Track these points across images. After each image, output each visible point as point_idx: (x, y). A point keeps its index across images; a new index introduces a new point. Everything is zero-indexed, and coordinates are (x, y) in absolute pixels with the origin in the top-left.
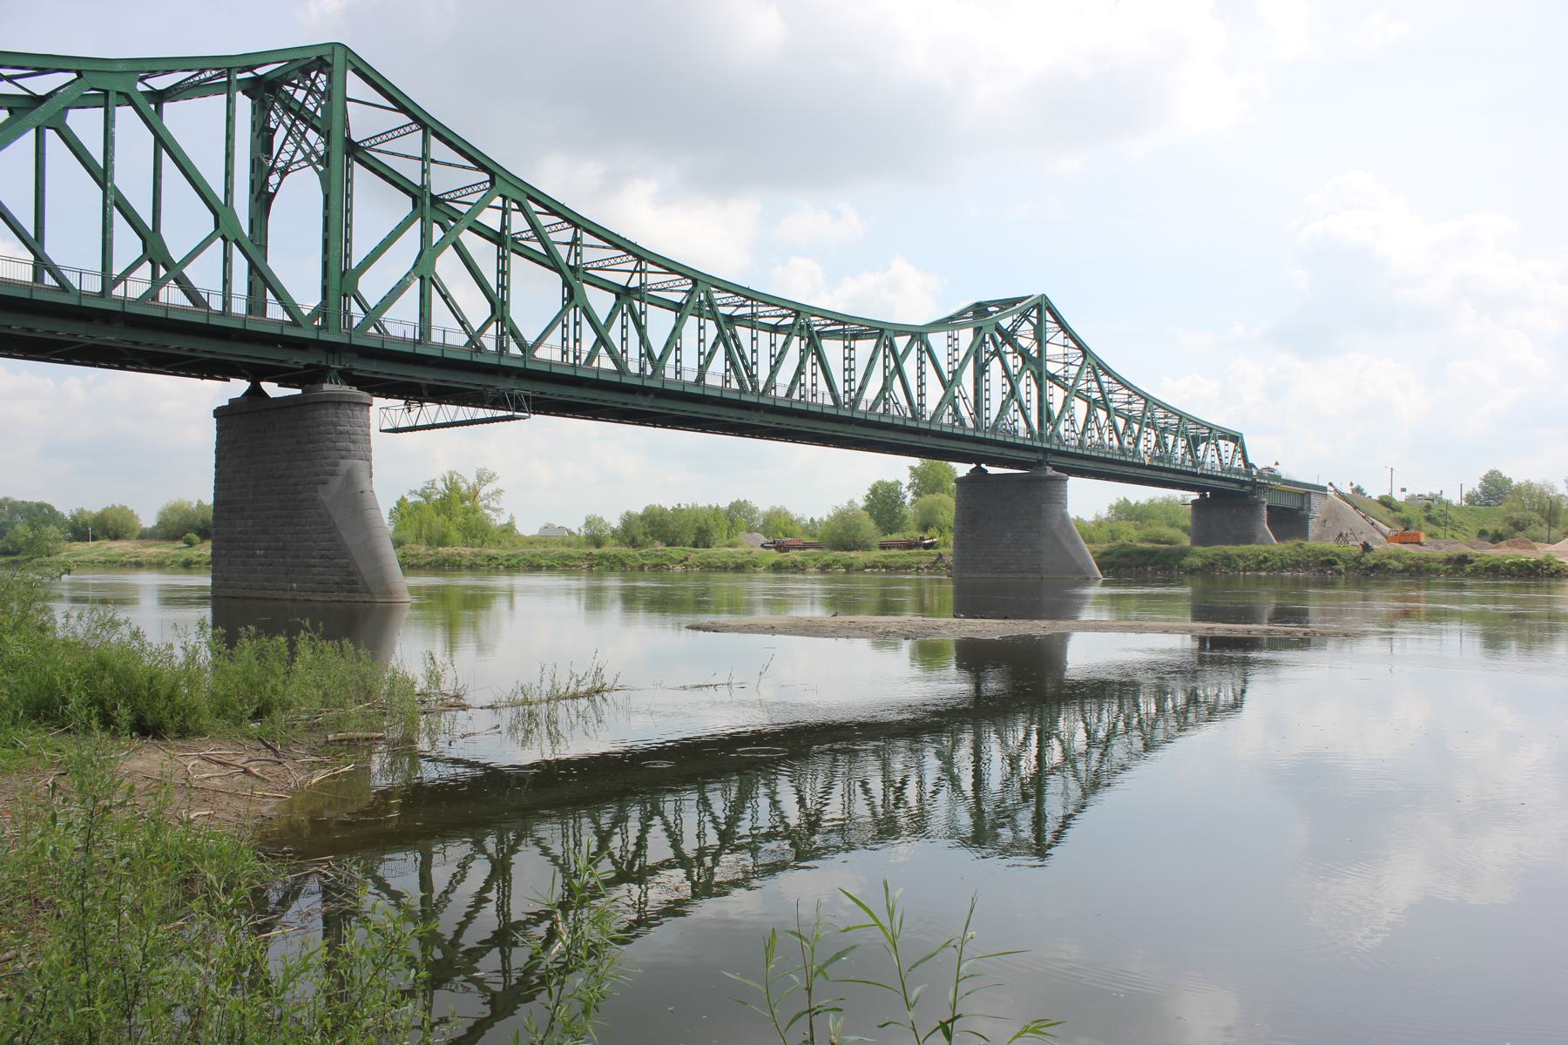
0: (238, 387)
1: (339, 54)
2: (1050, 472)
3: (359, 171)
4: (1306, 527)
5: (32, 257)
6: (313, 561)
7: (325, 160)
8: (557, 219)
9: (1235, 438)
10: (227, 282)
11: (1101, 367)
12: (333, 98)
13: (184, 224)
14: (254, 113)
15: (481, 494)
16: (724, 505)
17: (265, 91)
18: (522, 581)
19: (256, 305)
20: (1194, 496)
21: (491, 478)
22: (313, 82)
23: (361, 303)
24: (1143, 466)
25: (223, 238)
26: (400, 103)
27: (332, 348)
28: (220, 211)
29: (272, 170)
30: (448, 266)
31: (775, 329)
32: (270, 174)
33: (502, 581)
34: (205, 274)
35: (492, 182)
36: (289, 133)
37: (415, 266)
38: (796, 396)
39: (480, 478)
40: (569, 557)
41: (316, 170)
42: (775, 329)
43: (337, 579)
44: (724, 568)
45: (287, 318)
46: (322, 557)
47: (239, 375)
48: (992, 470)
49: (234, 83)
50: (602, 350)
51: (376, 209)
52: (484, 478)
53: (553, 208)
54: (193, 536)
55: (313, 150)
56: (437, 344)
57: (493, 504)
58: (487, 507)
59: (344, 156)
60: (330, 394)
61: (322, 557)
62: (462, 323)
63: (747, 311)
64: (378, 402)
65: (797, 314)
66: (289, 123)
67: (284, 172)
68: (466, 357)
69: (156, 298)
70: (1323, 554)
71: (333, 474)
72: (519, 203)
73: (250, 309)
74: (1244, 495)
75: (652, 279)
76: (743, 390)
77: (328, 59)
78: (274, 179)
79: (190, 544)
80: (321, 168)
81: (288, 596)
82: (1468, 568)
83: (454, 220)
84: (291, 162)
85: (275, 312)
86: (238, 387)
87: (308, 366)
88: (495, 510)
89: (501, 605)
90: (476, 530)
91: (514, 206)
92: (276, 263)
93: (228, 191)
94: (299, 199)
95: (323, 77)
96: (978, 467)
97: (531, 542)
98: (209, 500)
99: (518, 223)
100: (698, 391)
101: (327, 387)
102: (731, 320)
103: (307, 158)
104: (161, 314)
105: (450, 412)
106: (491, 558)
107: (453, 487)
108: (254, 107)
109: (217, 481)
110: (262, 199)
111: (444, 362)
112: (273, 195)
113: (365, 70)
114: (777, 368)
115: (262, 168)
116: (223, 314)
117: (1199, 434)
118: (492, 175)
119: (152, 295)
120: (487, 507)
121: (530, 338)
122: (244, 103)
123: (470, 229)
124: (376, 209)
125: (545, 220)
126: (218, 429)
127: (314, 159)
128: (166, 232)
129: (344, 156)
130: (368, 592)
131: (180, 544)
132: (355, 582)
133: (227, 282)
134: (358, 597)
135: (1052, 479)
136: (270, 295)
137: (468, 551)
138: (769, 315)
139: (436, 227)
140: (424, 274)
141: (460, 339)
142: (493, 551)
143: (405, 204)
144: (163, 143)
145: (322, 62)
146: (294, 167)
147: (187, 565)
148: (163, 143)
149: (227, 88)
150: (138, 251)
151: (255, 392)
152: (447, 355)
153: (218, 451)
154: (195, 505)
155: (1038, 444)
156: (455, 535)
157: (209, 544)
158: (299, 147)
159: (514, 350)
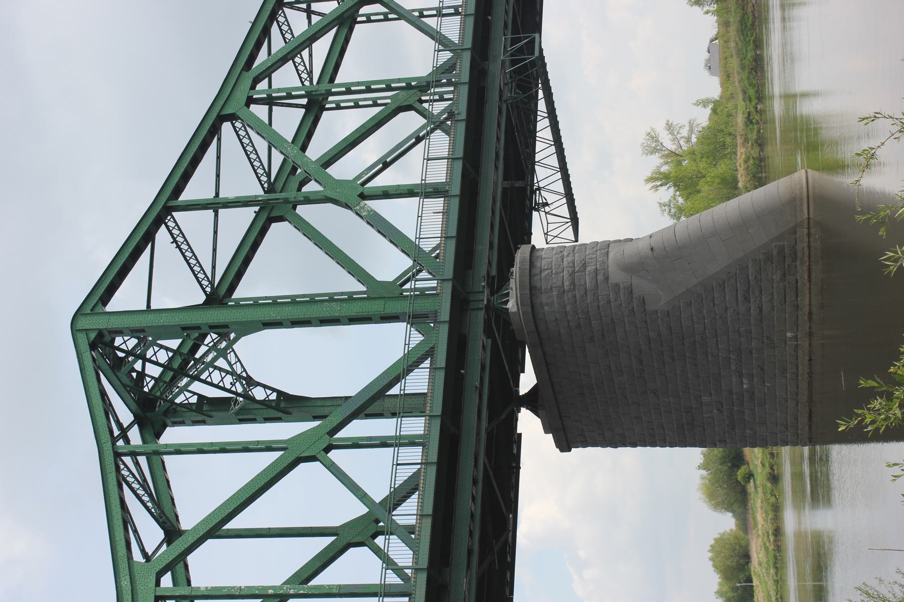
0: (528, 423)
1: (83, 323)
3: (240, 293)
6: (754, 312)
7: (223, 330)
8: (275, 29)
10: (383, 443)
12: (148, 326)
13: (313, 497)
14: (182, 423)
15: (672, 147)
17: (154, 412)
18: (776, 88)
19: (410, 406)
21: (653, 137)
22: (129, 353)
23: (409, 276)
25: (328, 449)
26: (141, 241)
27: (461, 303)
28: (293, 458)
29: (246, 396)
30: (347, 169)
32: (253, 399)
33: (777, 108)
34: (377, 472)
35: (232, 118)
36: (196, 378)
37: (347, 206)
39: (654, 151)
40: (742, 22)
41: (236, 340)
43: (777, 277)
45: (427, 363)
46: (747, 299)
47: (512, 421)
49: (151, 447)
51: (284, 267)
52: (653, 146)
53: (260, 34)
54: (741, 473)
55: (214, 347)
56: (450, 172)
57: (685, 132)
58: (688, 140)
59: (223, 311)
60: (521, 303)
61: (747, 299)
62: (419, 140)
64: (537, 239)
66: (186, 380)
67: (250, 382)
68: (461, 128)
69: (411, 529)
71: (630, 291)
72: (257, 80)
73: (420, 412)
77: (93, 336)
78: (259, 394)
79: (750, 476)
80: (232, 336)
81: (804, 343)
83: (294, 169)
84: (233, 373)
85: (418, 381)
86: (528, 423)
87: (488, 332)
88: (691, 131)
89: (808, 108)
90: (715, 144)
91: (263, 85)
92: (350, 383)
93: (268, 447)
94: (275, 359)
95: (118, 341)
97: (726, 78)
98: (694, 455)
99: (286, 78)
101: (511, 305)
103: (223, 354)
104: (428, 522)
105: (544, 151)
106: (749, 121)
107: (660, 179)
108: (175, 424)
109: (653, 445)
110: (286, 406)
111: (470, 160)
112: (280, 393)
113: (102, 290)
115: (242, 406)
118: (222, 118)
119: (406, 533)
120: (688, 140)
122: (172, 435)
123: (304, 148)
124: (284, 267)
125: (277, 43)
126: (585, 444)
127: (224, 344)
128: (336, 521)
129: (223, 311)
130: (794, 231)
131: (751, 487)
132: (781, 250)
133: (383, 443)
134: (802, 245)
135: (532, 291)
136: (395, 390)
137: (741, 151)
139: (305, 189)
140: (357, 196)
141: (440, 142)
142: (740, 119)
143: (280, 233)
144: (215, 529)
145: (100, 343)
146: (239, 370)
147: (775, 478)
148: (215, 529)
149: (156, 457)
150: (363, 552)
151: (533, 401)
152: (460, 153)
153: (615, 445)
154: (704, 472)
156: (722, 167)
157: (747, 451)
158: (211, 364)
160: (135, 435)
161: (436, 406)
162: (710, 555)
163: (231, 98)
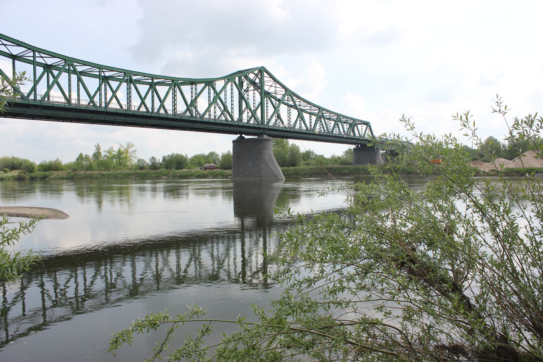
0: (239, 135)
2: (265, 137)
5: (89, 100)
9: (367, 124)
11: (295, 96)
16: (207, 153)
20: (353, 147)
24: (343, 138)
27: (264, 129)
44: (116, 177)
48: (246, 137)
50: (143, 105)
57: (134, 155)
58: (131, 156)
65: (173, 81)
75: (278, 89)
76: (192, 116)
88: (134, 157)
100: (248, 125)
114: (121, 98)
116: (99, 107)
117: (354, 123)
120: (131, 156)
135: (265, 140)
138: (121, 76)
141: (85, 101)
155: (261, 126)
162: (116, 149)
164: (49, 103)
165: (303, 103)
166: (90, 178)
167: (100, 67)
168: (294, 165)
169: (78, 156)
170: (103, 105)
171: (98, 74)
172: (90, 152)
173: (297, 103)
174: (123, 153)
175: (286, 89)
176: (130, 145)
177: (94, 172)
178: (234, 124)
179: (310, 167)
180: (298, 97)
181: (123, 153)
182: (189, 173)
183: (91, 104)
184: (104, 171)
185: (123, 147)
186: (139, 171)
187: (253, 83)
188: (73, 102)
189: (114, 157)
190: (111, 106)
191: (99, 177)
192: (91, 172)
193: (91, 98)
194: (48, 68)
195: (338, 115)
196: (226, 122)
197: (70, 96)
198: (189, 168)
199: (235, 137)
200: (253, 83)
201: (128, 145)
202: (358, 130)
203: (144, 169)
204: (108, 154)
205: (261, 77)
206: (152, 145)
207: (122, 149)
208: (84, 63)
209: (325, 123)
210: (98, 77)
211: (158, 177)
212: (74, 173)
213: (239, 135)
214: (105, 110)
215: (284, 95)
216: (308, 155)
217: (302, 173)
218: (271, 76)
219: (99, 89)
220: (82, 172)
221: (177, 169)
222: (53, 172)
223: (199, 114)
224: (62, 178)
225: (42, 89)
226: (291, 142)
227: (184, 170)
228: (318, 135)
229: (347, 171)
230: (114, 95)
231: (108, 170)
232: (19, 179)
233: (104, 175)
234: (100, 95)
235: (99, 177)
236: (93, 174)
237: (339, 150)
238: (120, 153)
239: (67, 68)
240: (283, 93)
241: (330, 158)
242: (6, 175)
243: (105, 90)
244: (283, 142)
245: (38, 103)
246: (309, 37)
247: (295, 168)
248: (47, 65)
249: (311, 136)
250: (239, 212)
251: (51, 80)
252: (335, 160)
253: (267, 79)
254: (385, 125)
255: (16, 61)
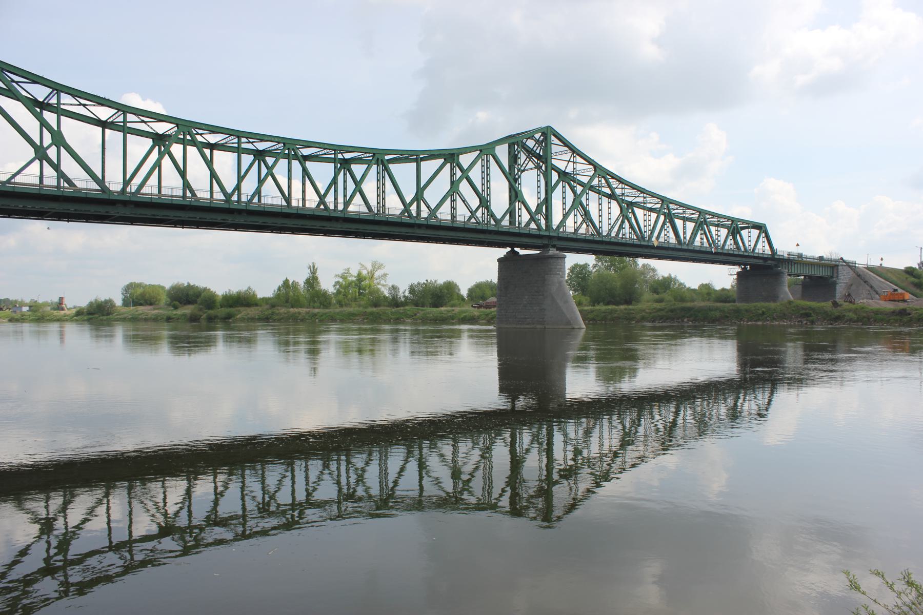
0: (509, 249)
2: (552, 251)
4: (835, 289)
5: (55, 174)
9: (761, 228)
11: (613, 178)
16: (441, 281)
27: (550, 237)
31: (651, 210)
38: (620, 235)
42: (651, 210)
48: (522, 252)
53: (614, 177)
56: (295, 207)
57: (383, 282)
63: (641, 199)
70: (803, 309)
74: (769, 267)
75: (579, 167)
76: (738, 248)
82: (905, 319)
88: (383, 286)
96: (513, 250)
100: (575, 237)
102: (631, 205)
111: (464, 229)
114: (371, 194)
116: (334, 210)
117: (735, 227)
121: (499, 216)
135: (552, 257)
138: (652, 203)
141: (312, 201)
144: (306, 173)
148: (306, 173)
159: (492, 222)
160: (340, 156)
161: (433, 221)
162: (354, 272)
163: (106, 147)
164: (41, 188)
165: (628, 191)
166: (295, 319)
167: (337, 149)
168: (628, 302)
169: (280, 283)
170: (341, 207)
171: (333, 156)
172: (300, 278)
173: (618, 191)
174: (365, 279)
175: (596, 167)
176: (376, 266)
177: (300, 310)
178: (552, 234)
179: (663, 305)
180: (620, 180)
181: (365, 279)
182: (450, 314)
183: (322, 207)
184: (319, 308)
185: (366, 268)
186: (370, 310)
187: (530, 153)
188: (294, 203)
189: (350, 284)
190: (351, 208)
191: (297, 315)
192: (296, 310)
193: (322, 198)
194: (260, 155)
195: (701, 212)
196: (537, 233)
197: (290, 194)
198: (452, 306)
199: (502, 252)
200: (530, 153)
201: (374, 266)
202: (742, 239)
203: (380, 306)
204: (341, 280)
205: (546, 144)
206: (406, 266)
207: (364, 272)
208: (210, 128)
209: (662, 226)
210: (334, 161)
211: (398, 321)
212: (270, 312)
213: (509, 249)
214: (342, 215)
215: (592, 178)
216: (667, 284)
217: (638, 316)
218: (566, 143)
219: (334, 181)
220: (283, 310)
221: (436, 306)
222: (241, 309)
223: (492, 215)
224: (253, 319)
225: (249, 186)
226: (641, 262)
227: (443, 309)
228: (658, 248)
229: (718, 314)
230: (359, 189)
231: (326, 307)
232: (193, 319)
233: (315, 315)
234: (336, 191)
235: (297, 315)
236: (299, 313)
237: (723, 277)
238: (360, 278)
239: (287, 152)
240: (591, 173)
241: (697, 288)
242: (175, 312)
243: (345, 182)
244: (623, 262)
245: (242, 206)
246: (699, 82)
247: (630, 307)
248: (157, 134)
249: (646, 250)
250: (510, 381)
251: (264, 171)
252: (706, 291)
253: (556, 147)
254: (803, 231)
255: (107, 131)
